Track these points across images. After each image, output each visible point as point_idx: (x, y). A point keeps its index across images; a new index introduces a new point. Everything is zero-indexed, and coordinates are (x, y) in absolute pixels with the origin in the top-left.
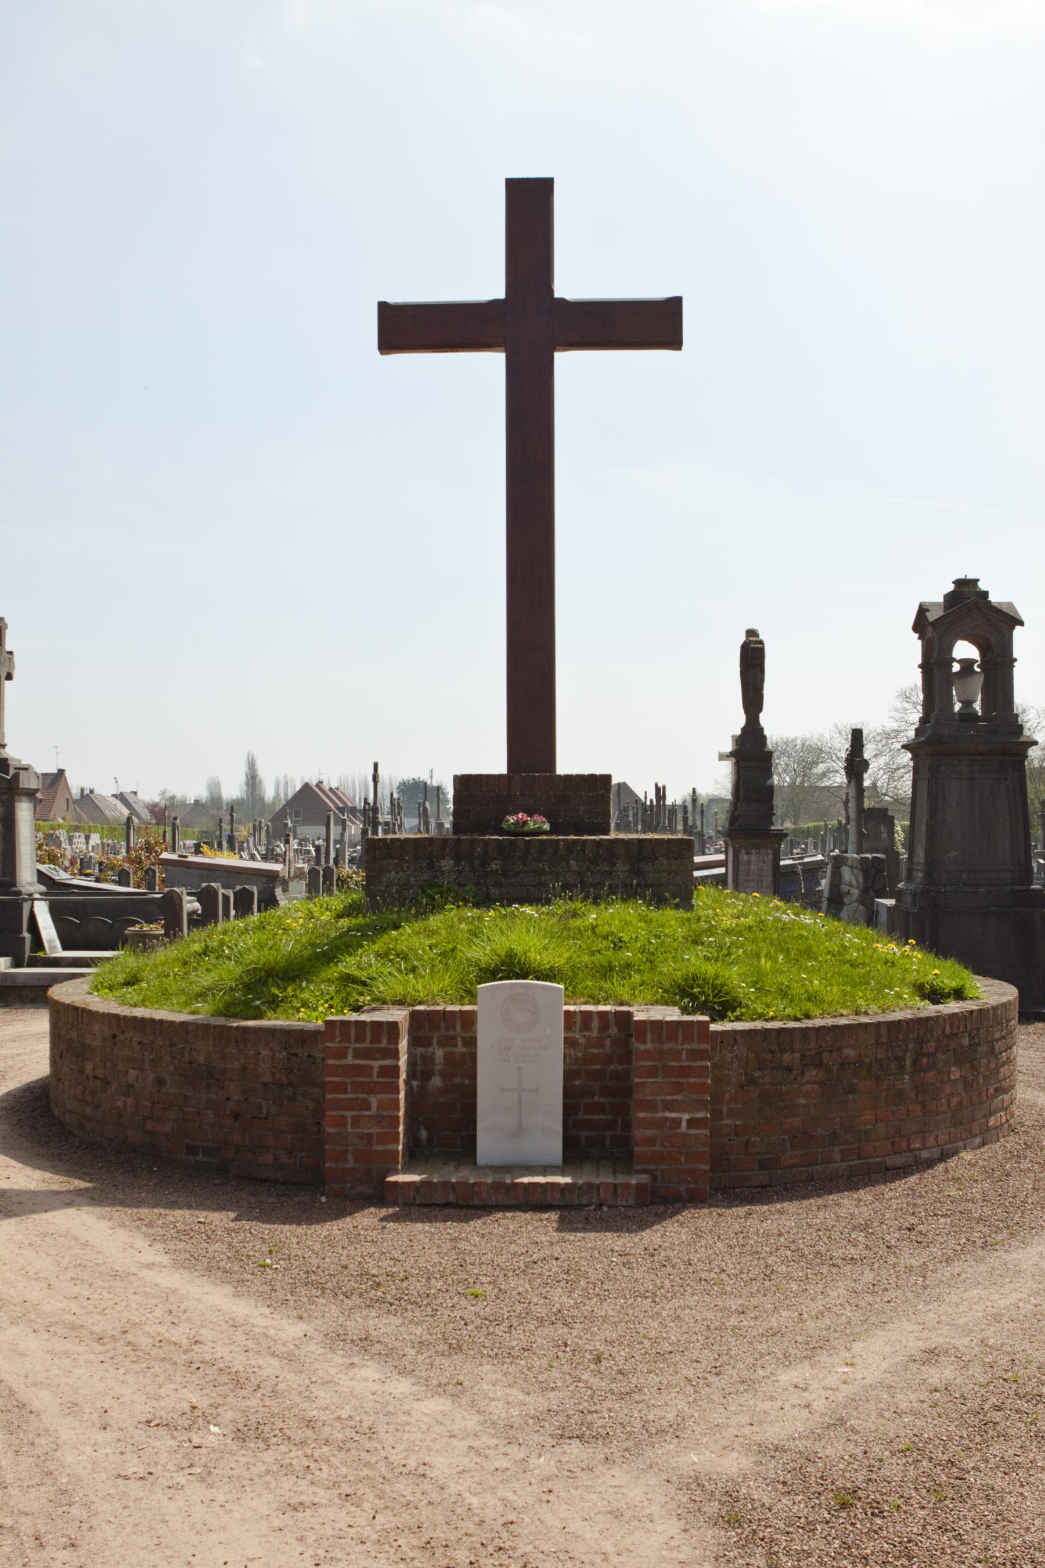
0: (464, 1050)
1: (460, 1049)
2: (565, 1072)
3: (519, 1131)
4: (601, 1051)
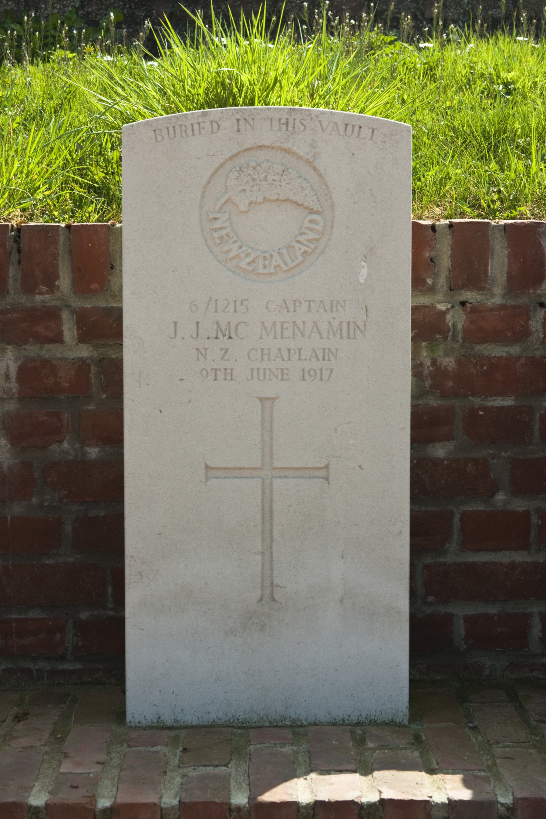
0: (84, 352)
1: (73, 348)
2: (412, 413)
3: (267, 606)
4: (515, 350)
